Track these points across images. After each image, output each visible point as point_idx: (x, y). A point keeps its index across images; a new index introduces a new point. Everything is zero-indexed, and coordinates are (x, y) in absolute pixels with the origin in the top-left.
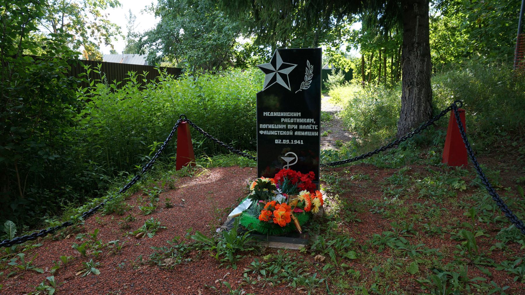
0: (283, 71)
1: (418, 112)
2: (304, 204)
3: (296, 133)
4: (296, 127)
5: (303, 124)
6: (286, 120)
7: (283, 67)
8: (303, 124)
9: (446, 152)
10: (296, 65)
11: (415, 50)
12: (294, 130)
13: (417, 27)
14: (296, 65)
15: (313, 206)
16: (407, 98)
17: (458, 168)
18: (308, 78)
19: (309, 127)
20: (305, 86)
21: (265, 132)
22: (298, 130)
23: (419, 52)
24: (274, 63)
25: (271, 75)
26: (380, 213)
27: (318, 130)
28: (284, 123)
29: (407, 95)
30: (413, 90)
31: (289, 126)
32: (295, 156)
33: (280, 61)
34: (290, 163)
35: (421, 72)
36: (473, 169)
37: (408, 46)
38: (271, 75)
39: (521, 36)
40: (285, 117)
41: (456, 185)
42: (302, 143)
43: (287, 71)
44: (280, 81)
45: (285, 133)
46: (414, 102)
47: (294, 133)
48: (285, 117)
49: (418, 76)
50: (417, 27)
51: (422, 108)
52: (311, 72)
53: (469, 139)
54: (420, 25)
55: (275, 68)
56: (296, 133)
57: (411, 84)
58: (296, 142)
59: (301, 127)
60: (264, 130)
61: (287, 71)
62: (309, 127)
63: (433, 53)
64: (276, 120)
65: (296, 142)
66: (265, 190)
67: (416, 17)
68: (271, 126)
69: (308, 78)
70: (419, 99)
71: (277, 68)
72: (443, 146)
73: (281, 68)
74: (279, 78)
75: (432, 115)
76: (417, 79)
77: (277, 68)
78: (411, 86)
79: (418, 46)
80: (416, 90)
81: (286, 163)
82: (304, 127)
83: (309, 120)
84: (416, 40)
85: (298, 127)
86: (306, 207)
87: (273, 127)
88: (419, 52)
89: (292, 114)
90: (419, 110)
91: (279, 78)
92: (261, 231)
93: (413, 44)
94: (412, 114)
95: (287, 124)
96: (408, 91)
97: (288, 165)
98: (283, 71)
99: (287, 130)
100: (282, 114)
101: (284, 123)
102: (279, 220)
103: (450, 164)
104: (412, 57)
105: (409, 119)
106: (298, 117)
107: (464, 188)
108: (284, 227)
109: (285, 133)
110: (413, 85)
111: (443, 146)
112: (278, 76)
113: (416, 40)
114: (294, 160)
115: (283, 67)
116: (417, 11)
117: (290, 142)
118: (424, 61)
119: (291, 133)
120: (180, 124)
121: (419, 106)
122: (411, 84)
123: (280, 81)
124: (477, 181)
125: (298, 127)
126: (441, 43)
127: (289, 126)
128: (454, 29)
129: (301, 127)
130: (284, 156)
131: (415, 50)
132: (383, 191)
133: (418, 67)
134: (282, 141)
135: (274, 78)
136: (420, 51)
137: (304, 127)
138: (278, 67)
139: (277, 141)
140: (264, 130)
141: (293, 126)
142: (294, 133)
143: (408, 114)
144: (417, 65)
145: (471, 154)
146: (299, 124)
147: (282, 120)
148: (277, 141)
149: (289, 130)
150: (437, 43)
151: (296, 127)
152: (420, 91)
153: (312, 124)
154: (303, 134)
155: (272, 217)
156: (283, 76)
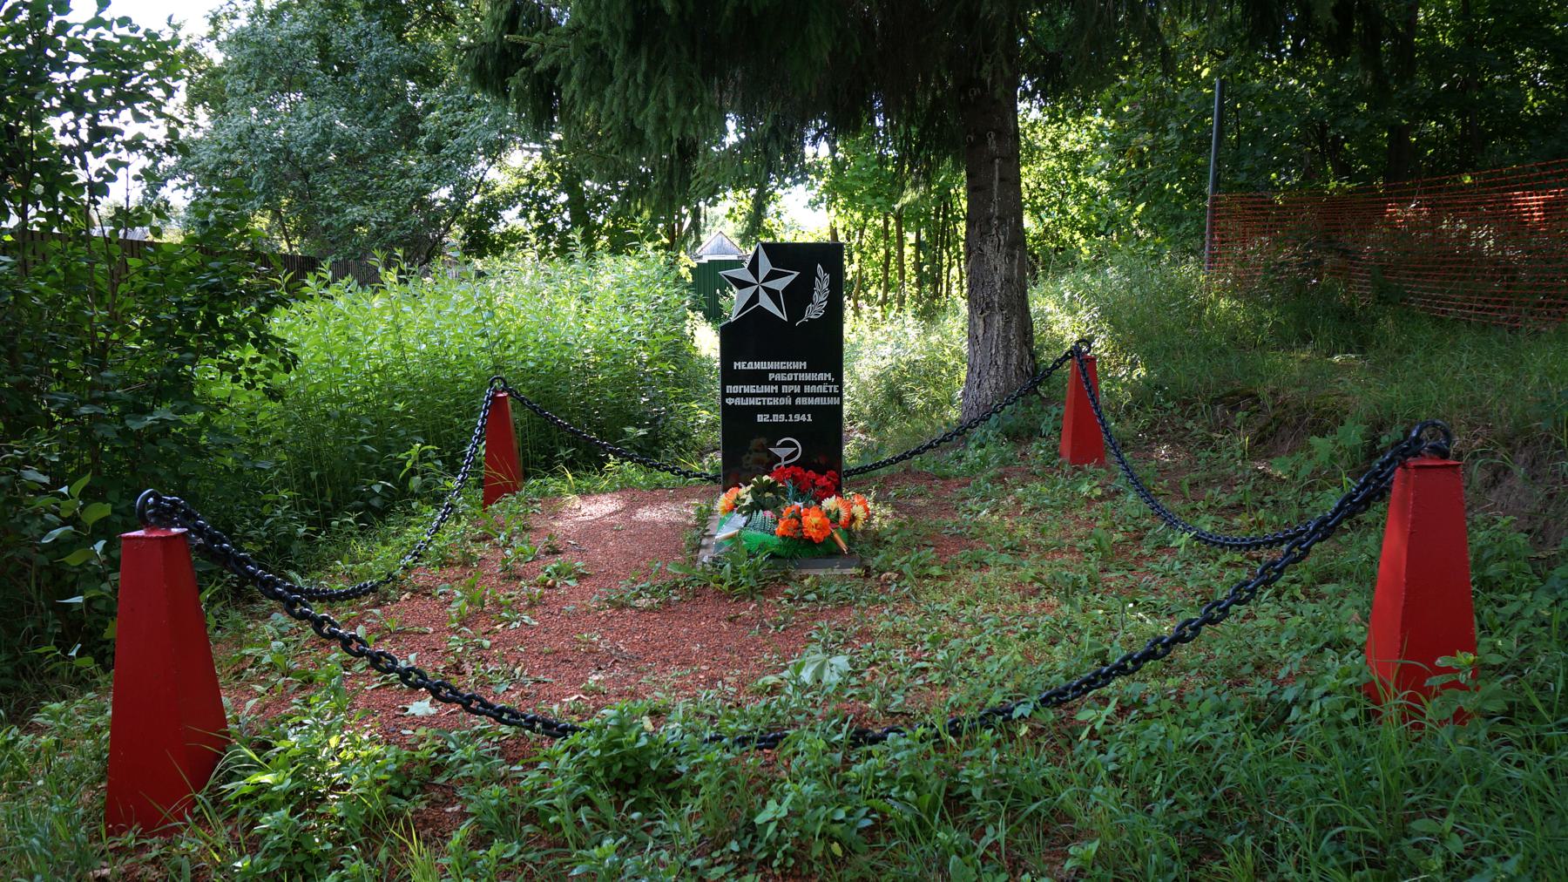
0: (771, 284)
1: (1006, 369)
2: (838, 515)
3: (798, 401)
4: (797, 389)
5: (811, 383)
6: (778, 377)
7: (772, 276)
8: (811, 383)
9: (1065, 447)
10: (797, 273)
11: (994, 232)
12: (794, 395)
13: (996, 183)
14: (797, 273)
15: (853, 518)
16: (980, 339)
17: (1088, 467)
18: (820, 297)
19: (822, 389)
20: (814, 311)
21: (738, 401)
22: (802, 394)
23: (1002, 237)
24: (754, 267)
25: (749, 291)
26: (961, 534)
27: (840, 395)
28: (774, 383)
29: (980, 332)
30: (992, 321)
31: (785, 389)
32: (795, 446)
33: (765, 266)
34: (786, 459)
35: (1008, 280)
36: (1114, 467)
37: (977, 224)
38: (749, 291)
39: (1217, 199)
40: (776, 371)
41: (1085, 489)
42: (810, 420)
43: (780, 284)
44: (766, 302)
45: (776, 401)
46: (997, 346)
47: (793, 401)
48: (776, 371)
49: (1002, 289)
50: (996, 183)
51: (1014, 360)
52: (825, 286)
53: (1108, 417)
54: (1001, 180)
55: (757, 278)
56: (798, 401)
57: (987, 307)
58: (798, 418)
59: (807, 389)
60: (734, 396)
61: (780, 284)
62: (822, 389)
63: (1028, 222)
64: (760, 377)
65: (798, 418)
66: (768, 495)
67: (992, 162)
68: (748, 389)
69: (820, 297)
70: (1007, 339)
71: (761, 280)
72: (1060, 437)
73: (767, 279)
74: (763, 296)
75: (1034, 375)
76: (1000, 296)
77: (761, 280)
78: (987, 313)
79: (1000, 225)
80: (998, 320)
81: (779, 460)
82: (814, 389)
83: (822, 376)
84: (994, 210)
85: (802, 389)
86: (842, 520)
87: (753, 391)
88: (1002, 237)
89: (788, 365)
90: (1006, 363)
91: (763, 296)
92: (783, 552)
93: (988, 220)
94: (992, 373)
95: (780, 383)
96: (981, 323)
97: (783, 463)
98: (771, 284)
99: (780, 395)
100: (771, 365)
101: (774, 383)
102: (813, 533)
103: (1073, 461)
104: (988, 249)
105: (986, 385)
106: (802, 371)
107: (1098, 492)
108: (819, 544)
109: (776, 401)
110: (993, 309)
111: (1060, 437)
112: (762, 294)
113: (994, 210)
114: (795, 453)
115: (772, 276)
116: (994, 148)
117: (787, 417)
118: (1013, 256)
119: (789, 401)
120: (493, 398)
121: (1007, 356)
122: (987, 307)
123: (766, 302)
124: (1120, 484)
125: (802, 389)
126: (1043, 190)
127: (785, 389)
128: (1076, 157)
129: (807, 389)
130: (775, 446)
131: (994, 232)
132: (956, 509)
133: (1002, 270)
134: (771, 418)
135: (755, 298)
136: (1004, 234)
137: (814, 389)
138: (762, 276)
139: (760, 418)
140: (734, 396)
141: (791, 388)
142: (793, 401)
143: (984, 373)
144: (999, 264)
145: (1114, 448)
146: (802, 383)
147: (771, 376)
148: (760, 418)
149: (785, 395)
150: (1034, 191)
151: (797, 389)
152: (1007, 322)
153: (830, 383)
154: (811, 401)
155: (799, 528)
156: (772, 294)
